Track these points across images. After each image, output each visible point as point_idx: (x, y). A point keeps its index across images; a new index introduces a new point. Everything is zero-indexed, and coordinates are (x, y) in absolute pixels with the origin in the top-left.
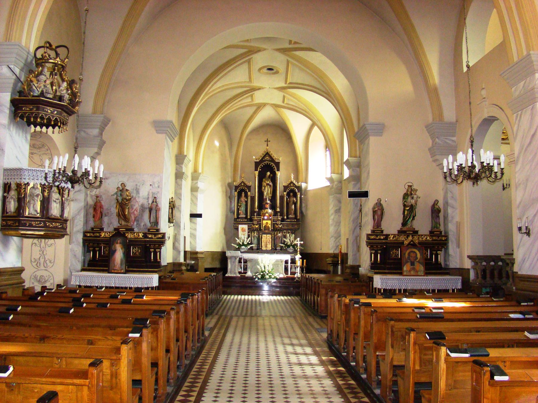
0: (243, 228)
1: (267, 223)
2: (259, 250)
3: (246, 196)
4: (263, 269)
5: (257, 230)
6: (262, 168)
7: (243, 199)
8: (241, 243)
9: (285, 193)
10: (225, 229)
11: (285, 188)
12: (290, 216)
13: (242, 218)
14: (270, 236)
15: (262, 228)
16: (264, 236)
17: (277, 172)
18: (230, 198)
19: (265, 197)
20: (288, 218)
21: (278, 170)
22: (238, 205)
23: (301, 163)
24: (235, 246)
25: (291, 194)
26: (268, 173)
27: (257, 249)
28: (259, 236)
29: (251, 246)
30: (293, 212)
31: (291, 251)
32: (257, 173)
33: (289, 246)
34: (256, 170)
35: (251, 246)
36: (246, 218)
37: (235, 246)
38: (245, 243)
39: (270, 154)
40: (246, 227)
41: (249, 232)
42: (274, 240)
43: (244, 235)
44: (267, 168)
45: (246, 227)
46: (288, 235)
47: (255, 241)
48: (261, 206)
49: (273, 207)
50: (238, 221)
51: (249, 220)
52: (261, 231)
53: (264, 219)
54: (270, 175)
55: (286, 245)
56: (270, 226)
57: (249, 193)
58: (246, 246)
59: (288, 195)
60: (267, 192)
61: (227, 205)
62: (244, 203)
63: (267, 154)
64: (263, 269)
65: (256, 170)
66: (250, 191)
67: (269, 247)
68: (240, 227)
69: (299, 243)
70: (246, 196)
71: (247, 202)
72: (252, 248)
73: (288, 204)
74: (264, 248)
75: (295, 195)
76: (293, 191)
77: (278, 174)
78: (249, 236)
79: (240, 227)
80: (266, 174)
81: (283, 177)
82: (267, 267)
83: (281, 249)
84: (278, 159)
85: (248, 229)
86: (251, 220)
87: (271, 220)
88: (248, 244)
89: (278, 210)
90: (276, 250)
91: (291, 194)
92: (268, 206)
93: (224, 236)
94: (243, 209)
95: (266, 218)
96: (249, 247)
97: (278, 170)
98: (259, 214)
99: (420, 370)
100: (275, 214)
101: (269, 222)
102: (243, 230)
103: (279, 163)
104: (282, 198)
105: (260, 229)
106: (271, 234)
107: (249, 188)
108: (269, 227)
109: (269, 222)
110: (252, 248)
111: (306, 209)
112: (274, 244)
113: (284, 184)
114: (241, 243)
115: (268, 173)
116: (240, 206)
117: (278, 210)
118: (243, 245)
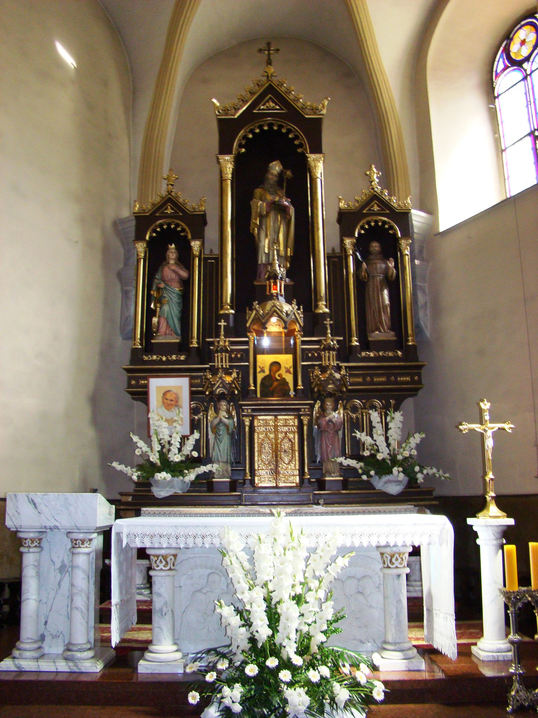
0: (169, 389)
1: (276, 365)
2: (234, 490)
3: (185, 258)
4: (263, 632)
5: (230, 396)
6: (248, 143)
7: (172, 270)
8: (154, 458)
9: (348, 242)
10: (95, 400)
11: (346, 220)
12: (376, 336)
13: (166, 349)
14: (292, 420)
15: (255, 386)
16: (263, 420)
17: (311, 157)
18: (124, 279)
19: (262, 259)
20: (365, 345)
21: (317, 149)
22: (149, 298)
23: (400, 138)
24: (128, 470)
25: (375, 246)
26: (276, 167)
27: (233, 486)
28: (241, 424)
29: (203, 469)
30: (385, 318)
31: (394, 489)
32: (228, 164)
33: (384, 468)
34: (225, 149)
35: (203, 469)
36: (183, 347)
37: (128, 470)
38: (175, 457)
39: (282, 90)
40: (181, 385)
41: (194, 411)
42: (310, 440)
43: (170, 421)
44: (270, 147)
45: (181, 385)
46: (375, 416)
47: (222, 448)
48: (252, 290)
49: (301, 290)
50: (144, 361)
51: (192, 356)
52: (250, 394)
53: (258, 350)
54: (281, 175)
55: (372, 462)
56: (289, 378)
57: (196, 245)
58: (176, 469)
59: (362, 245)
60: (273, 245)
61: (107, 303)
62: (177, 289)
63: (271, 91)
64: (263, 632)
65: (225, 149)
66: (199, 235)
67: (290, 475)
68: (157, 385)
69: (490, 429)
70: (185, 258)
71: (186, 285)
72: (206, 483)
73: (361, 285)
74: (264, 479)
75: (391, 249)
76: (378, 229)
77: (319, 167)
78: (194, 425)
79: (157, 385)
80: (266, 170)
81: (332, 183)
82: (288, 610)
83: (345, 484)
84: (315, 110)
85: (193, 395)
86: (205, 354)
87: (292, 351)
88: (191, 462)
89: (323, 308)
90: (321, 485)
91: (375, 246)
92: (278, 288)
93: (90, 433)
94: (170, 309)
95: (266, 342)
96: (191, 476)
97: (317, 149)
98: (239, 328)
99: (501, 685)
100: (313, 325)
101: (286, 360)
102: (170, 401)
103: (318, 123)
104: (336, 262)
105: (246, 393)
106: (296, 412)
107: (198, 222)
108: (284, 382)
109: (286, 360)
110: (206, 483)
111: (437, 311)
112: (312, 460)
113: (342, 205)
114: (154, 458)
115: (276, 167)
116: (159, 301)
117: (323, 308)
118: (166, 464)
